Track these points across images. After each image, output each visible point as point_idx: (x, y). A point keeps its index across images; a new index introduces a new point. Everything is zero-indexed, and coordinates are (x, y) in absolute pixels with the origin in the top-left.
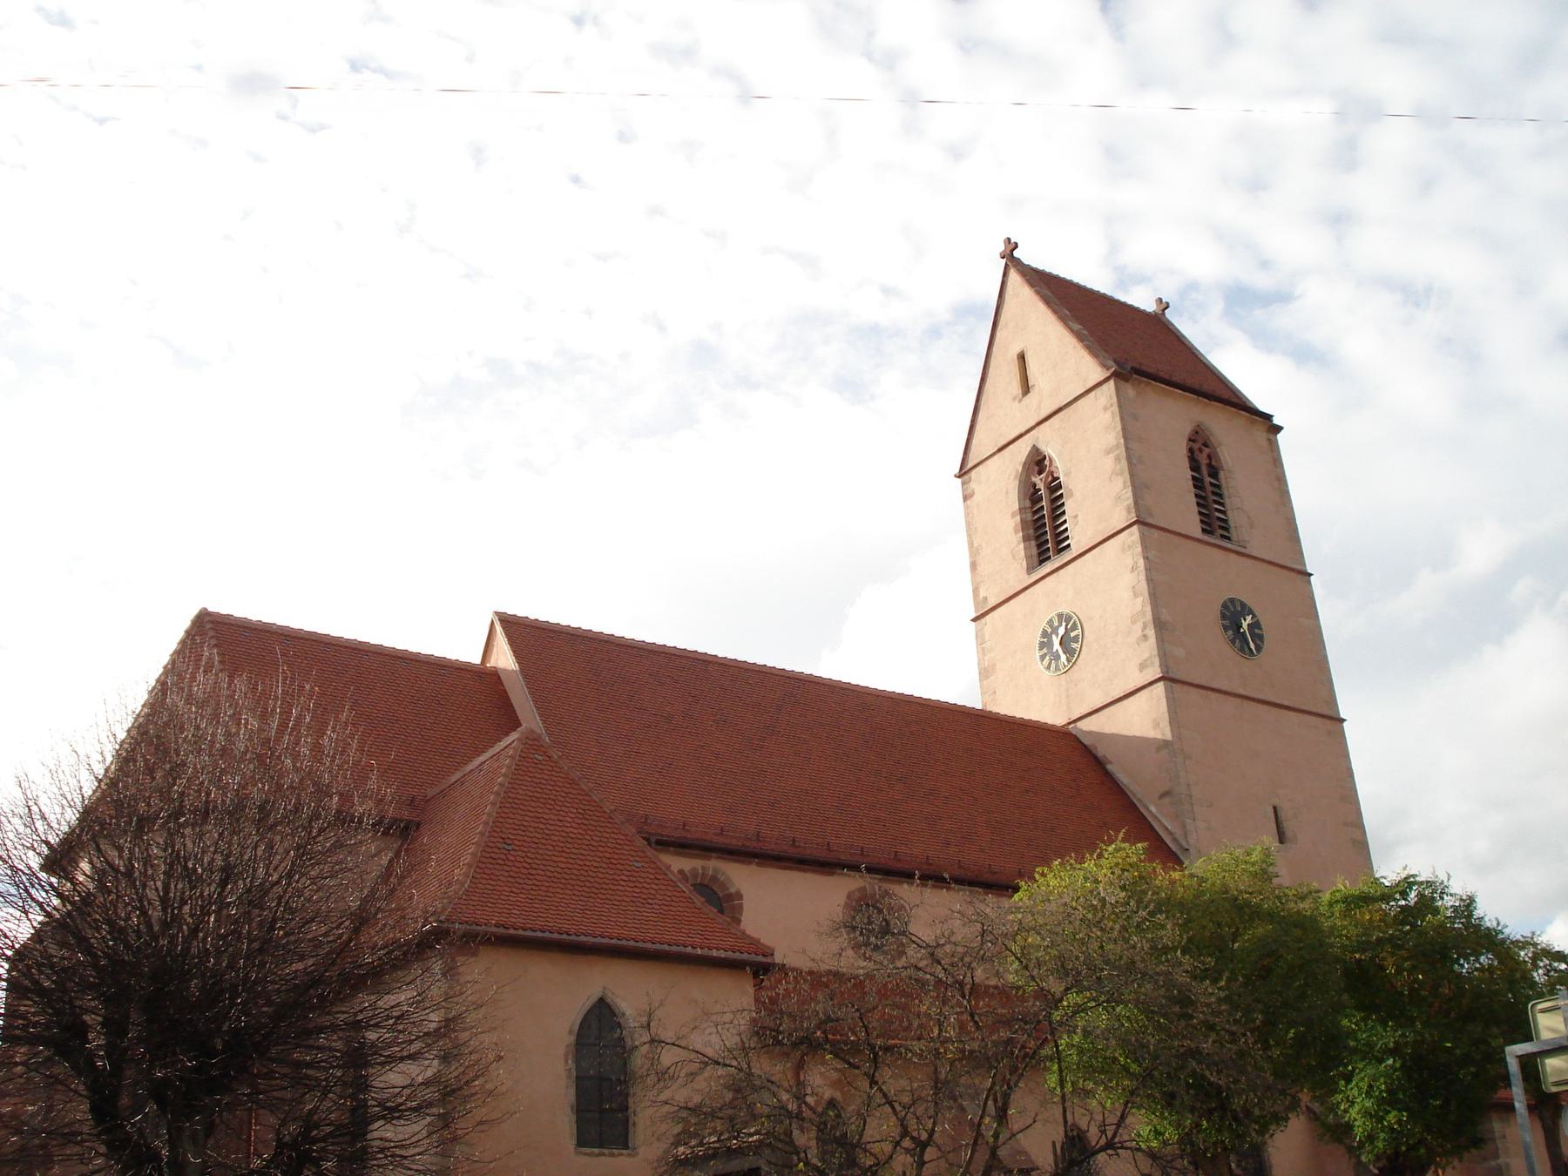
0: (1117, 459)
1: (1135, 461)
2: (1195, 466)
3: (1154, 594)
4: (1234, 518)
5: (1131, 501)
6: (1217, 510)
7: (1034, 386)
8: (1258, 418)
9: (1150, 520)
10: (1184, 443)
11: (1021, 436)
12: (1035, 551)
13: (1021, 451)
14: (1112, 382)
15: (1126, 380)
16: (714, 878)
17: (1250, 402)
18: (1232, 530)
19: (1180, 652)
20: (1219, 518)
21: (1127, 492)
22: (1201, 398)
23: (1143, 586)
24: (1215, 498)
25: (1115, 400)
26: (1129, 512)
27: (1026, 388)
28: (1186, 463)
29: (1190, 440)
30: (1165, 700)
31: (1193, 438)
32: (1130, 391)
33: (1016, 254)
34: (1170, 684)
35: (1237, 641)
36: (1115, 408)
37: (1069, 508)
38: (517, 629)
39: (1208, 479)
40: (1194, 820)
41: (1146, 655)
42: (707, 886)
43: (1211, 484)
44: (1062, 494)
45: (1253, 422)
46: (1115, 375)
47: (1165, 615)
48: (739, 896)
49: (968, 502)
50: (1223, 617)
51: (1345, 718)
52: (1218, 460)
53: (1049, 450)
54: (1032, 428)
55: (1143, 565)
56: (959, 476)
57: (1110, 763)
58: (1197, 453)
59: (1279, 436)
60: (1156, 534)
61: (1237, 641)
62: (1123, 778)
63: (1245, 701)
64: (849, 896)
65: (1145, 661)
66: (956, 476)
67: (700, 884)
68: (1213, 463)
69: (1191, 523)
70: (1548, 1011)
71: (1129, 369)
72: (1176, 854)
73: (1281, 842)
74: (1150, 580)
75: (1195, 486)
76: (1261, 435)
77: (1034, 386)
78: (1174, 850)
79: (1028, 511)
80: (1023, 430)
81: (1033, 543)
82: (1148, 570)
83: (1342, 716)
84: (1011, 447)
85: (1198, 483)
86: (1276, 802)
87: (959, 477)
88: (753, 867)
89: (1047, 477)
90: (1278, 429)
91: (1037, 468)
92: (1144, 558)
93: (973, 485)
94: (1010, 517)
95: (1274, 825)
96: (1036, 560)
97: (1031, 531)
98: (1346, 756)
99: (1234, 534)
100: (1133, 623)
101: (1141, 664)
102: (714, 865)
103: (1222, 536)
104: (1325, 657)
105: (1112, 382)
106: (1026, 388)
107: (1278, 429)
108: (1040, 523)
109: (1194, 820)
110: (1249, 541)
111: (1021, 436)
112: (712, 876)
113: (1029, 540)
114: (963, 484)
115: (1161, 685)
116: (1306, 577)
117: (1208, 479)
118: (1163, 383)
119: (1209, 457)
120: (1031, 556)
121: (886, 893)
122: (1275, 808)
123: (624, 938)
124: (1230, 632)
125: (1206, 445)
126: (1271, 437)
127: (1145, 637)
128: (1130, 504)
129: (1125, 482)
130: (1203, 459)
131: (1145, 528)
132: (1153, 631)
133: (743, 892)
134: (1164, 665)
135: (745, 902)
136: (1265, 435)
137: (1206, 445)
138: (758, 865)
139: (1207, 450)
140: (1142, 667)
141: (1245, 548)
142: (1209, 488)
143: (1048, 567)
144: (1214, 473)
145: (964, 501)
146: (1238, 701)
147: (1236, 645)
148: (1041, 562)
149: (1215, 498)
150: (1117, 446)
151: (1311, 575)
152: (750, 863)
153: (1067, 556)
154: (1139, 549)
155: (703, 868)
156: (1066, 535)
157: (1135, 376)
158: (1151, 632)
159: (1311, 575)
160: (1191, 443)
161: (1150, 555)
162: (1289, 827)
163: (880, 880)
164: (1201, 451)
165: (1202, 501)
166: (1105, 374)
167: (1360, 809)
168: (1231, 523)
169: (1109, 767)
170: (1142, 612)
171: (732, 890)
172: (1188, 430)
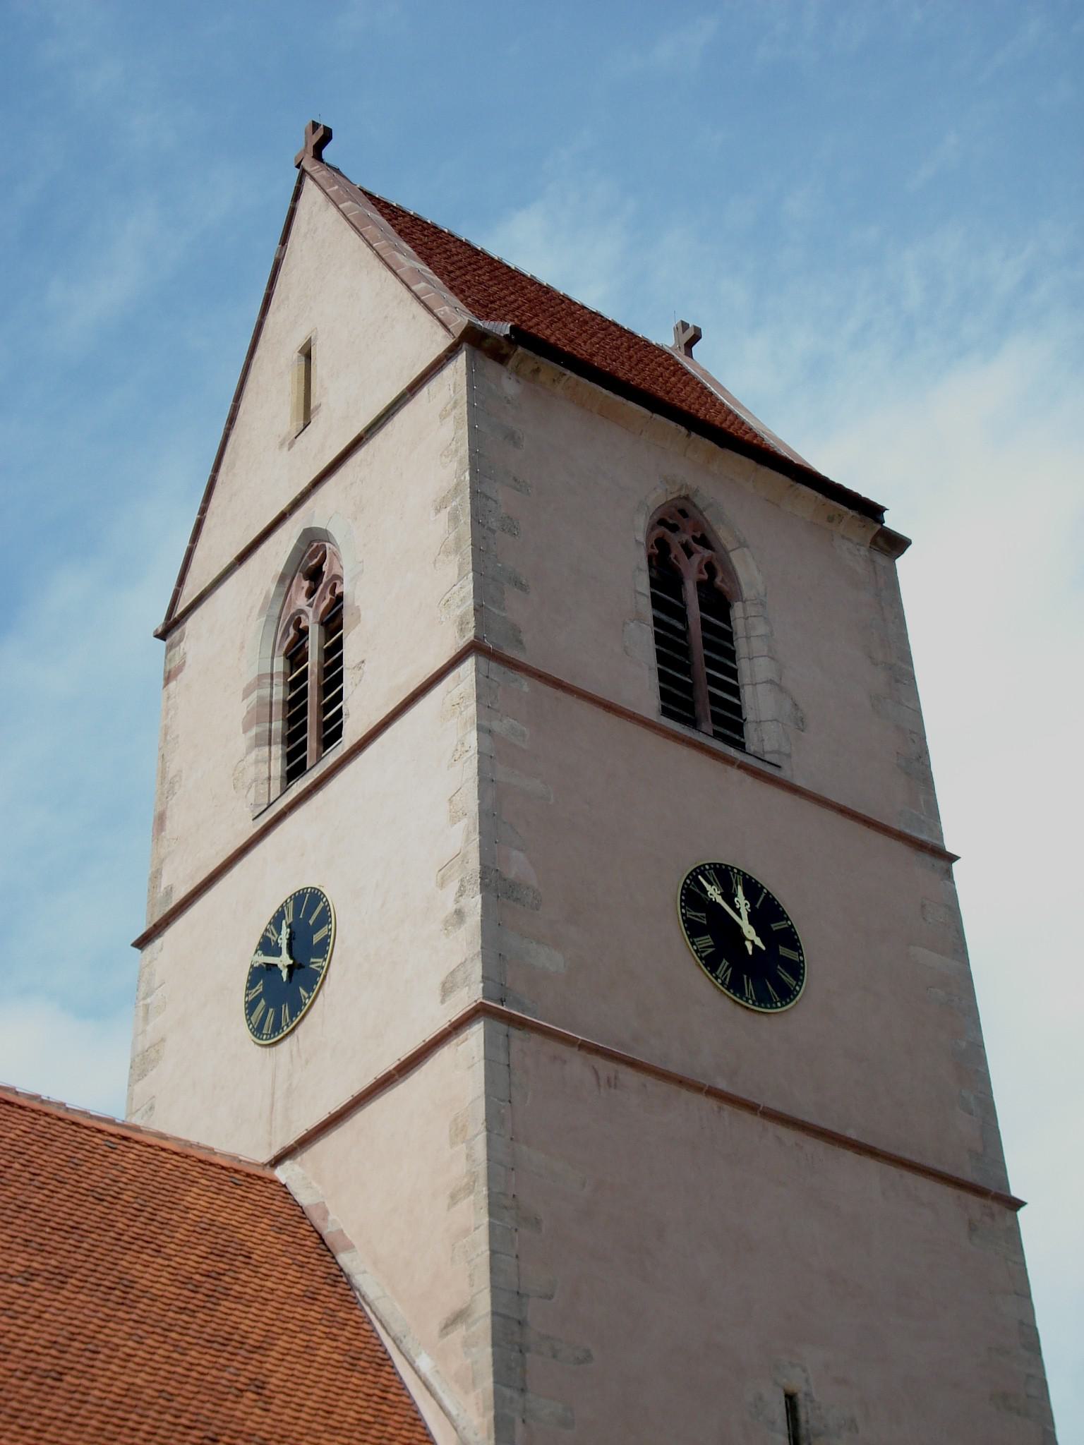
0: (454, 518)
1: (493, 523)
9: (510, 652)
10: (641, 523)
14: (457, 369)
15: (501, 358)
18: (749, 729)
19: (549, 960)
27: (307, 413)
29: (662, 522)
30: (482, 1063)
32: (508, 385)
34: (502, 1027)
35: (725, 963)
40: (523, 1391)
41: (457, 960)
46: (472, 339)
47: (518, 866)
52: (731, 575)
55: (474, 744)
57: (349, 1247)
58: (676, 551)
59: (900, 562)
63: (727, 1108)
65: (452, 973)
70: (420, 1377)
74: (486, 780)
81: (278, 750)
82: (487, 761)
83: (1015, 1192)
86: (797, 1383)
90: (897, 544)
91: (306, 584)
92: (480, 729)
98: (1022, 1292)
99: (751, 736)
100: (442, 884)
101: (444, 984)
106: (307, 413)
107: (897, 544)
109: (523, 1391)
110: (789, 756)
114: (169, 648)
116: (941, 864)
119: (710, 568)
122: (791, 1401)
126: (881, 560)
127: (459, 914)
128: (466, 614)
131: (493, 665)
132: (479, 898)
137: (704, 541)
139: (702, 554)
140: (447, 990)
146: (711, 1104)
147: (720, 971)
151: (1018, 1204)
154: (472, 709)
158: (474, 903)
160: (662, 529)
166: (440, 342)
168: (749, 714)
169: (344, 1259)
170: (461, 856)
172: (657, 496)
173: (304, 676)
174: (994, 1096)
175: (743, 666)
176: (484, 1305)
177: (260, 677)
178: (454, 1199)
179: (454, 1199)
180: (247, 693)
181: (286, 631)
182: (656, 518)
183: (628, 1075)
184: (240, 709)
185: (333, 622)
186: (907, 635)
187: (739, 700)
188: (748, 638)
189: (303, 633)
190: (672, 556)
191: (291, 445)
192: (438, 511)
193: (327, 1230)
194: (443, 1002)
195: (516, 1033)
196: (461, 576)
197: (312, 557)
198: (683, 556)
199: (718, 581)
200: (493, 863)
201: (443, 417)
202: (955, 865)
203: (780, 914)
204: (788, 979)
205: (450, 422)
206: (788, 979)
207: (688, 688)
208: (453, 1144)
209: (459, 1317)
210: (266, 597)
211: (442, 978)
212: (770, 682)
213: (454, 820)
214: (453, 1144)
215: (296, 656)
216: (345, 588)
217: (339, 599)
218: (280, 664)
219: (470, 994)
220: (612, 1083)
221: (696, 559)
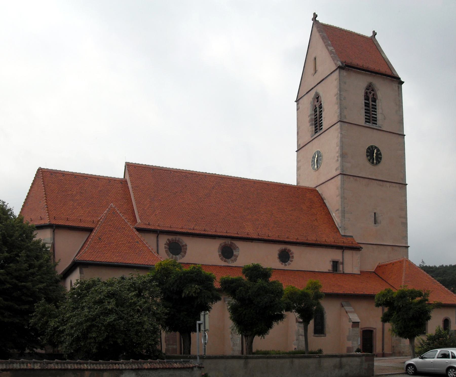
1: (342, 99)
2: (367, 98)
3: (342, 146)
4: (379, 117)
5: (339, 114)
6: (373, 114)
7: (317, 70)
8: (394, 79)
11: (313, 88)
12: (314, 129)
13: (312, 93)
16: (178, 241)
17: (396, 72)
20: (373, 117)
21: (338, 111)
22: (372, 74)
23: (339, 143)
24: (373, 110)
25: (338, 77)
26: (338, 117)
27: (316, 71)
28: (363, 98)
29: (367, 89)
31: (368, 88)
33: (317, 19)
34: (343, 176)
36: (338, 80)
37: (324, 114)
38: (129, 167)
39: (371, 103)
42: (177, 243)
43: (372, 105)
44: (322, 110)
45: (393, 81)
48: (186, 245)
49: (298, 111)
50: (367, 152)
51: (407, 184)
52: (377, 96)
53: (321, 94)
54: (315, 87)
56: (296, 101)
57: (325, 199)
58: (369, 94)
60: (346, 125)
61: (371, 160)
62: (327, 204)
63: (370, 180)
64: (220, 245)
65: (337, 168)
66: (295, 102)
67: (175, 242)
68: (374, 97)
69: (360, 118)
71: (344, 65)
72: (338, 228)
73: (375, 223)
75: (365, 106)
76: (395, 85)
77: (317, 70)
78: (337, 227)
79: (313, 115)
80: (313, 86)
81: (314, 126)
84: (310, 92)
85: (367, 105)
86: (375, 211)
87: (296, 102)
88: (191, 237)
89: (319, 103)
91: (316, 100)
92: (340, 134)
93: (299, 105)
94: (308, 117)
95: (373, 219)
96: (314, 132)
97: (313, 122)
99: (378, 122)
101: (336, 169)
102: (178, 237)
103: (373, 123)
104: (405, 163)
105: (338, 70)
106: (316, 71)
108: (316, 119)
109: (344, 218)
111: (313, 88)
112: (178, 240)
113: (313, 125)
115: (340, 176)
116: (403, 136)
117: (371, 103)
118: (358, 69)
119: (373, 95)
120: (313, 131)
121: (233, 243)
122: (375, 213)
123: (116, 262)
124: (369, 157)
125: (373, 90)
126: (399, 86)
127: (338, 160)
129: (338, 107)
130: (371, 96)
133: (187, 244)
134: (342, 170)
135: (188, 247)
136: (397, 85)
137: (373, 90)
138: (192, 237)
139: (373, 92)
140: (336, 170)
141: (381, 127)
142: (371, 106)
143: (317, 134)
144: (374, 100)
145: (297, 110)
146: (368, 180)
148: (316, 133)
149: (373, 110)
150: (337, 94)
151: (405, 135)
152: (190, 236)
153: (321, 131)
155: (175, 238)
156: (321, 124)
157: (346, 67)
158: (340, 159)
159: (405, 135)
160: (367, 90)
161: (343, 133)
162: (379, 219)
163: (230, 240)
164: (370, 93)
165: (367, 112)
166: (334, 68)
167: (407, 213)
169: (324, 201)
171: (184, 244)
173: (317, 114)
174: (408, 241)
175: (377, 111)
176: (340, 209)
177: (311, 114)
178: (337, 196)
179: (337, 196)
180: (309, 116)
181: (314, 108)
182: (366, 89)
183: (358, 178)
184: (308, 119)
185: (321, 107)
186: (406, 188)
187: (376, 104)
188: (378, 106)
189: (316, 108)
190: (368, 94)
191: (313, 76)
192: (335, 96)
193: (323, 197)
194: (336, 171)
195: (345, 176)
196: (338, 109)
197: (317, 95)
198: (369, 94)
199: (374, 97)
200: (343, 172)
201: (336, 80)
202: (405, 136)
203: (380, 154)
204: (380, 160)
205: (336, 81)
206: (380, 160)
207: (369, 104)
208: (337, 190)
209: (338, 210)
210: (311, 101)
211: (336, 168)
212: (381, 113)
213: (337, 146)
214: (337, 190)
215: (316, 111)
216: (322, 103)
217: (321, 104)
218: (313, 112)
219: (338, 172)
220: (356, 180)
221: (371, 94)
